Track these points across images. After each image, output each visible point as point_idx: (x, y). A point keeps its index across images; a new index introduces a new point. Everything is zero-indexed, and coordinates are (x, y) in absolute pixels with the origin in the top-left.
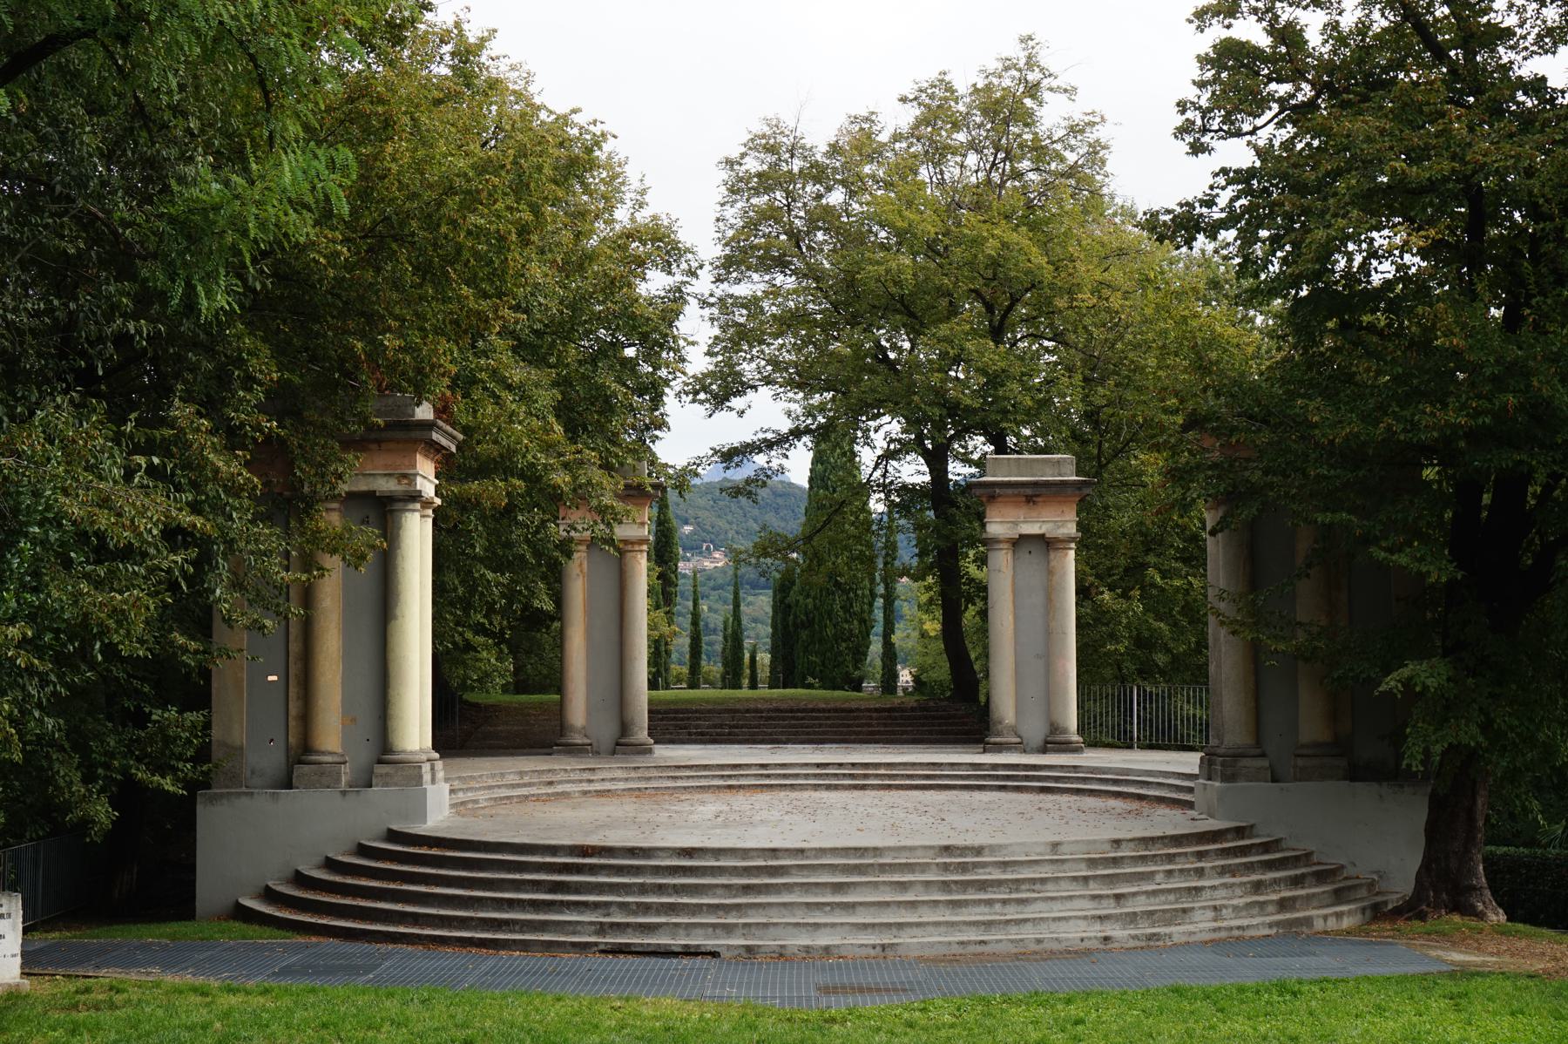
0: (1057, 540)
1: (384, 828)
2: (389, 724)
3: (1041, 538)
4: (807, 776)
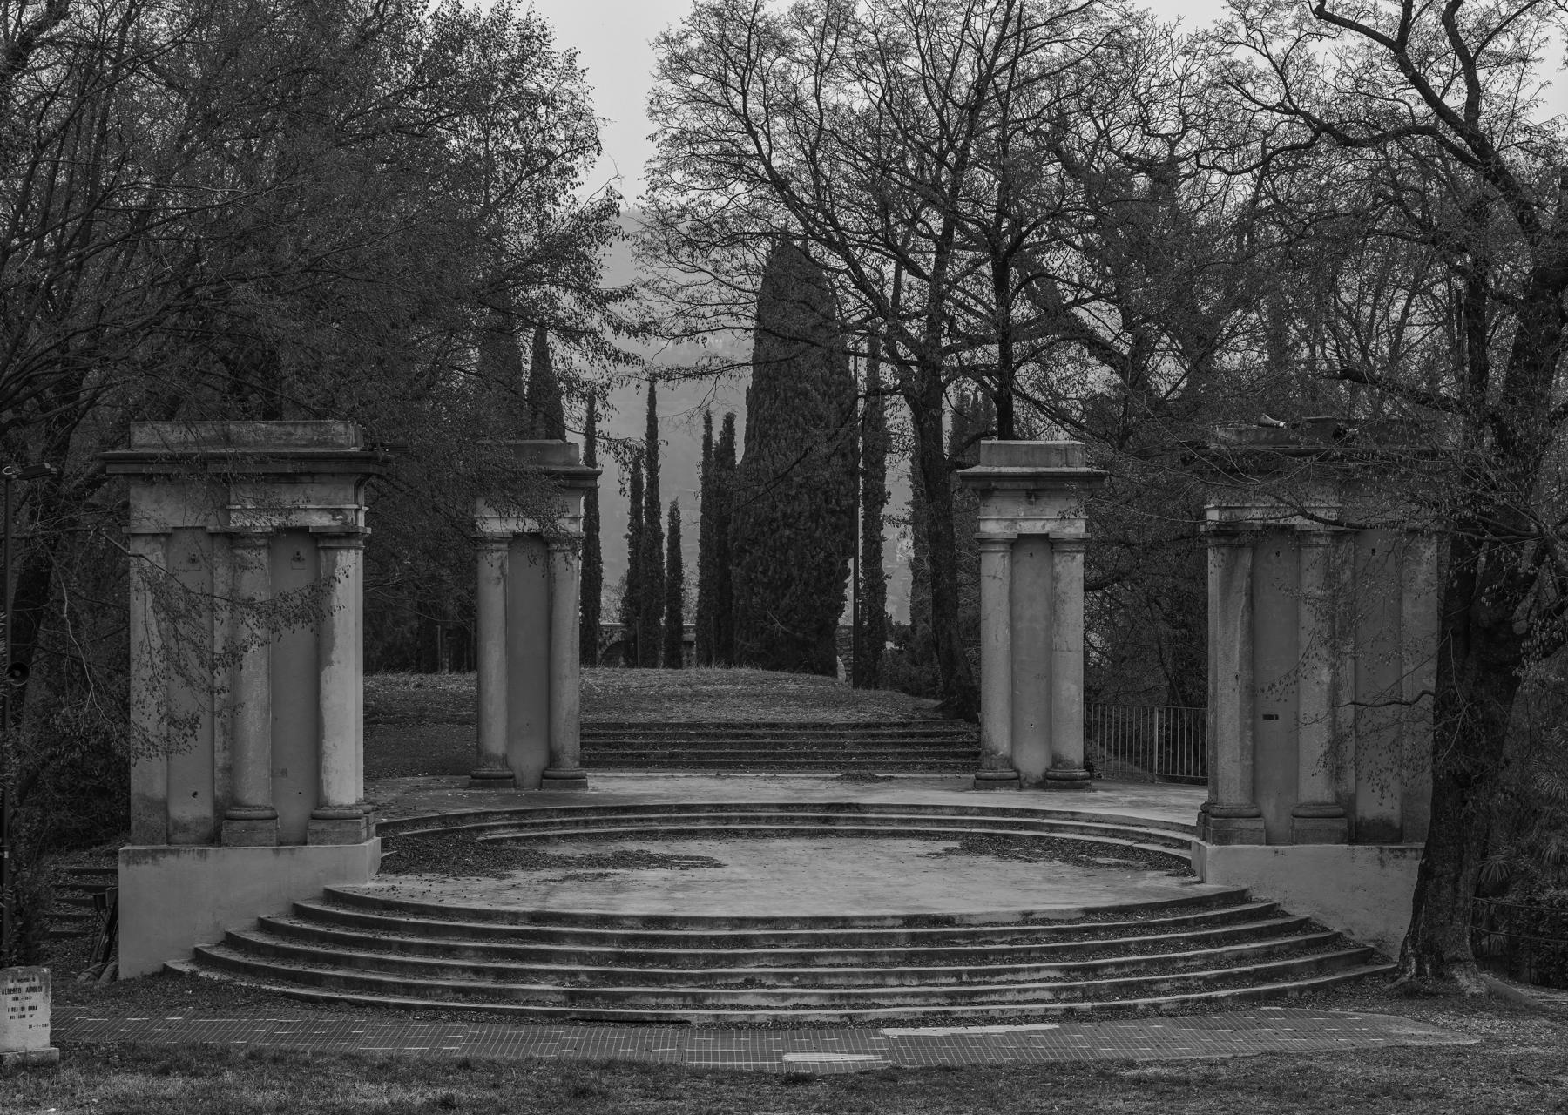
0: (1062, 541)
1: (321, 888)
2: (324, 777)
3: (1044, 538)
4: (768, 820)
